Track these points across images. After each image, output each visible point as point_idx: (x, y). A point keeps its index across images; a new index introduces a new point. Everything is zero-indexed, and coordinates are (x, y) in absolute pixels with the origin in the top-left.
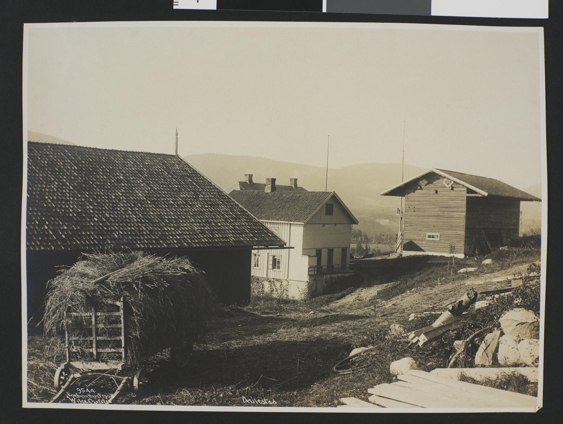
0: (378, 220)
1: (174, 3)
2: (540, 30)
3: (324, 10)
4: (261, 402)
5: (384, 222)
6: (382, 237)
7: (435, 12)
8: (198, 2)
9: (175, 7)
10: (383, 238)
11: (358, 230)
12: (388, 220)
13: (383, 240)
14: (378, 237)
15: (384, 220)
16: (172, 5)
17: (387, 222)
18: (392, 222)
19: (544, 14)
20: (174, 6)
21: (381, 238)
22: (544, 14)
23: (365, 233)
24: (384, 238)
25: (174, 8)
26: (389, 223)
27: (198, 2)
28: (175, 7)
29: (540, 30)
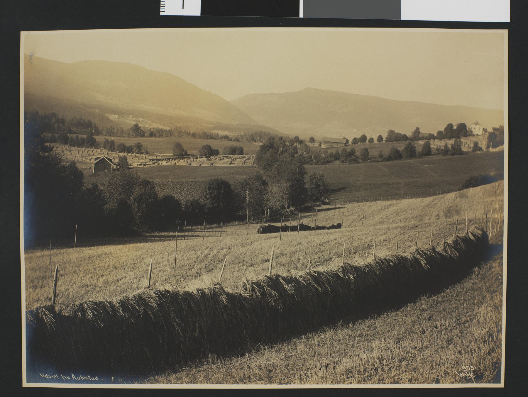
0: (107, 115)
1: (161, 10)
2: (505, 32)
3: (301, 15)
4: (85, 378)
5: (114, 117)
6: (113, 130)
7: (404, 16)
8: (183, 9)
9: (162, 14)
10: (114, 131)
11: (88, 120)
12: (117, 116)
13: (114, 133)
14: (109, 130)
15: (113, 115)
16: (159, 12)
17: (116, 117)
18: (121, 118)
19: (507, 18)
20: (161, 12)
21: (111, 131)
22: (507, 18)
23: (96, 125)
24: (115, 131)
25: (161, 15)
26: (118, 118)
27: (183, 9)
28: (162, 14)
29: (505, 32)
